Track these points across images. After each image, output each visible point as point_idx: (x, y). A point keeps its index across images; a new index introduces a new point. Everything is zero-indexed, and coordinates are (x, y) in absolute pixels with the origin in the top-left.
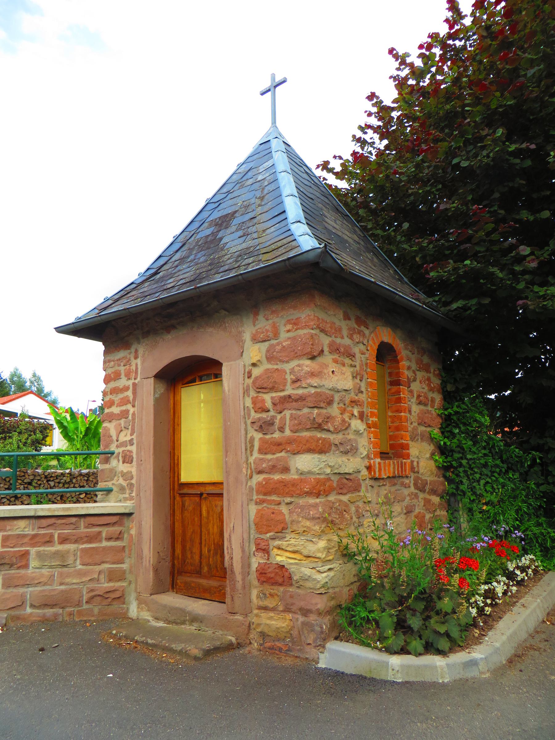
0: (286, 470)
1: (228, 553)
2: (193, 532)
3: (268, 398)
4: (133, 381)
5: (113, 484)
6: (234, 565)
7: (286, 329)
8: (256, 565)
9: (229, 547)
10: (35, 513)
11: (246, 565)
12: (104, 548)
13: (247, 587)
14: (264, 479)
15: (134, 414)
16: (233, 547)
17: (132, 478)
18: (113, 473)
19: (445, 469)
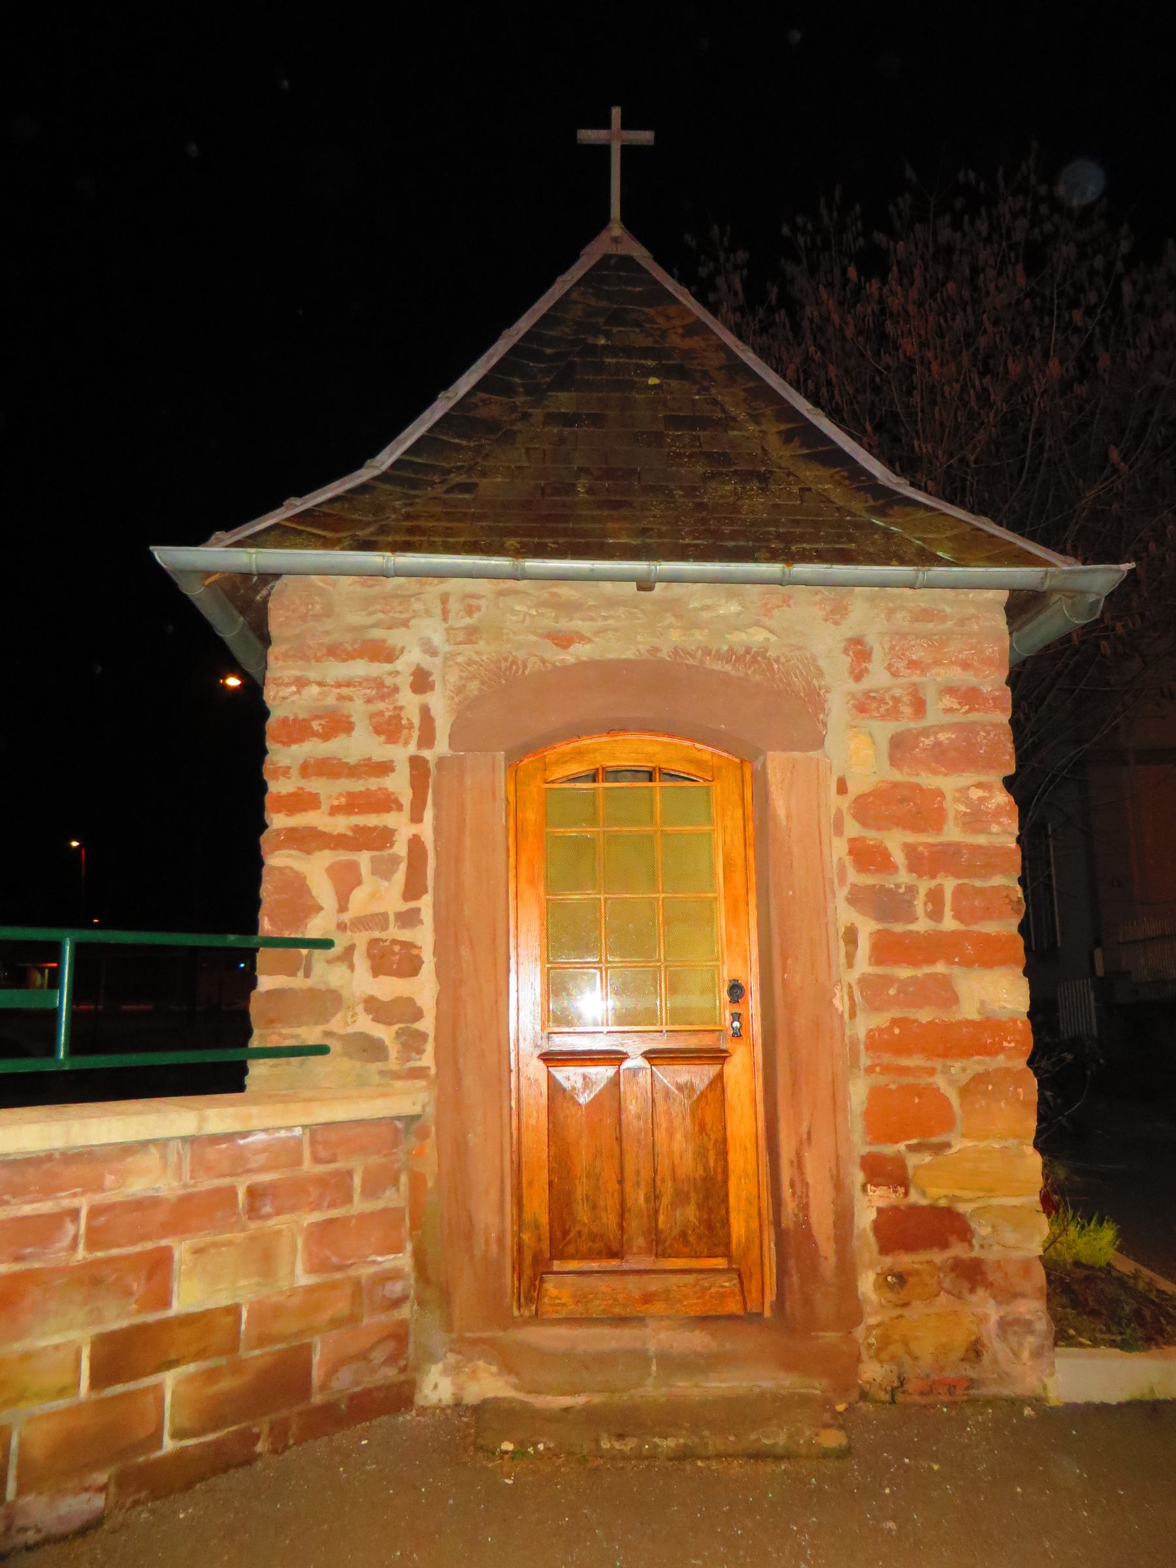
0: (951, 999)
1: (794, 1194)
2: (597, 1154)
3: (895, 842)
4: (412, 749)
5: (328, 1034)
6: (814, 1219)
7: (941, 706)
8: (873, 1215)
9: (797, 1180)
10: (200, 1128)
11: (844, 1217)
12: (362, 1217)
13: (847, 1270)
14: (895, 1022)
15: (415, 843)
16: (810, 1180)
17: (418, 1015)
18: (327, 1002)
19: (731, 651)
